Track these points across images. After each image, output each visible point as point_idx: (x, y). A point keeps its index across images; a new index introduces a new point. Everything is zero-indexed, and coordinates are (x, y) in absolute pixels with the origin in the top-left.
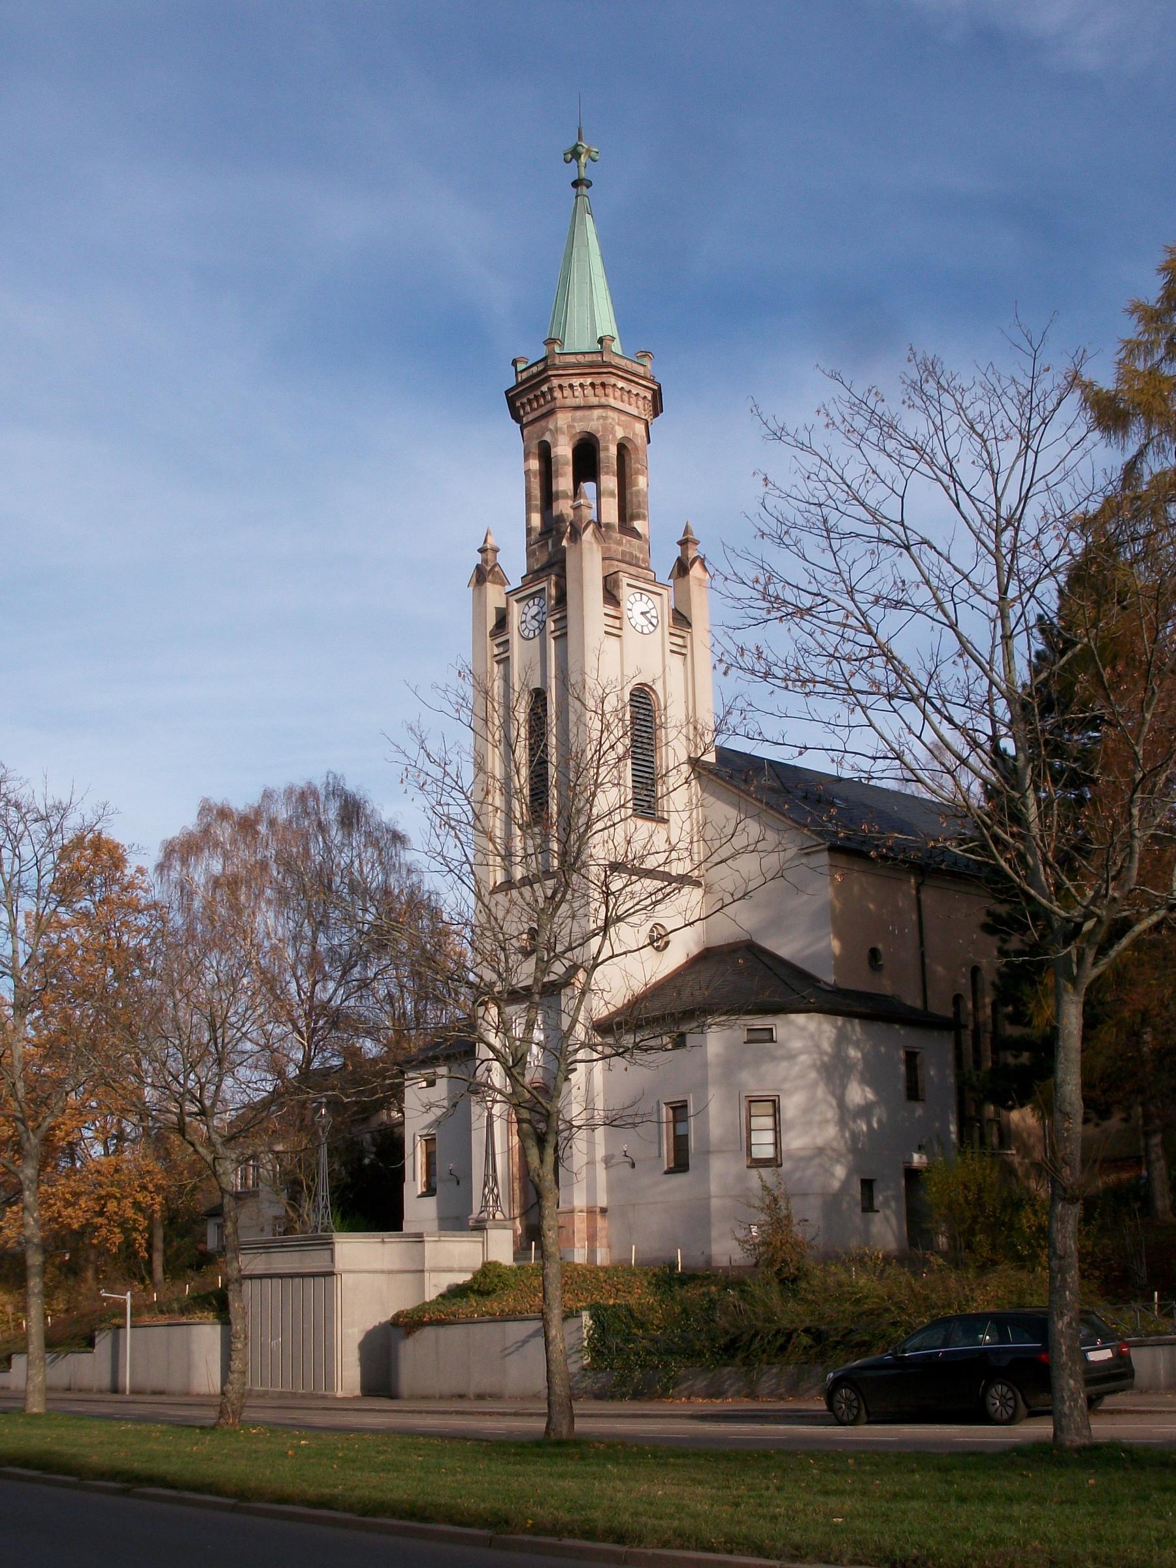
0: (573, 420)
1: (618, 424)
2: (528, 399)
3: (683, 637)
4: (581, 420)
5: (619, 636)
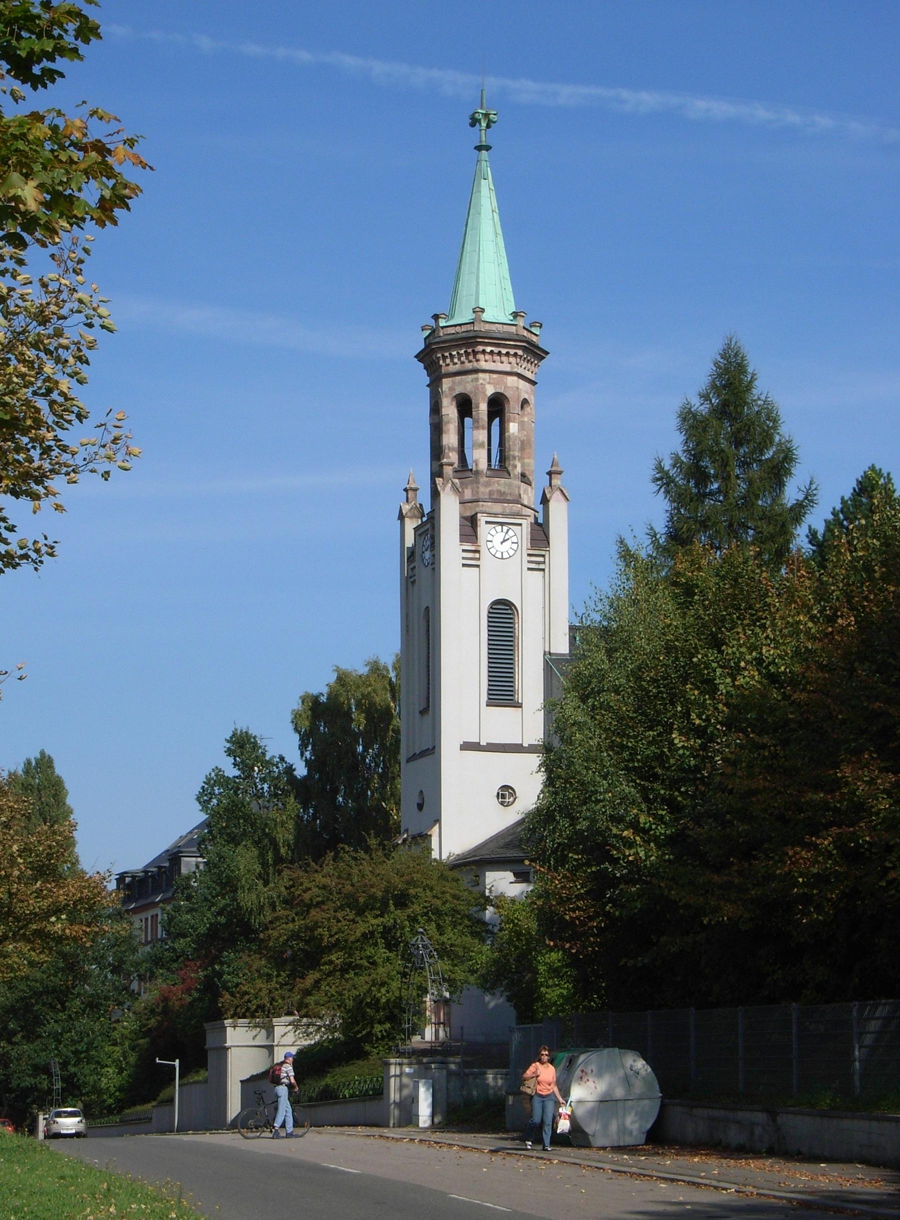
0: (454, 383)
1: (489, 383)
2: (465, 352)
3: (543, 556)
4: (460, 383)
5: (478, 566)
